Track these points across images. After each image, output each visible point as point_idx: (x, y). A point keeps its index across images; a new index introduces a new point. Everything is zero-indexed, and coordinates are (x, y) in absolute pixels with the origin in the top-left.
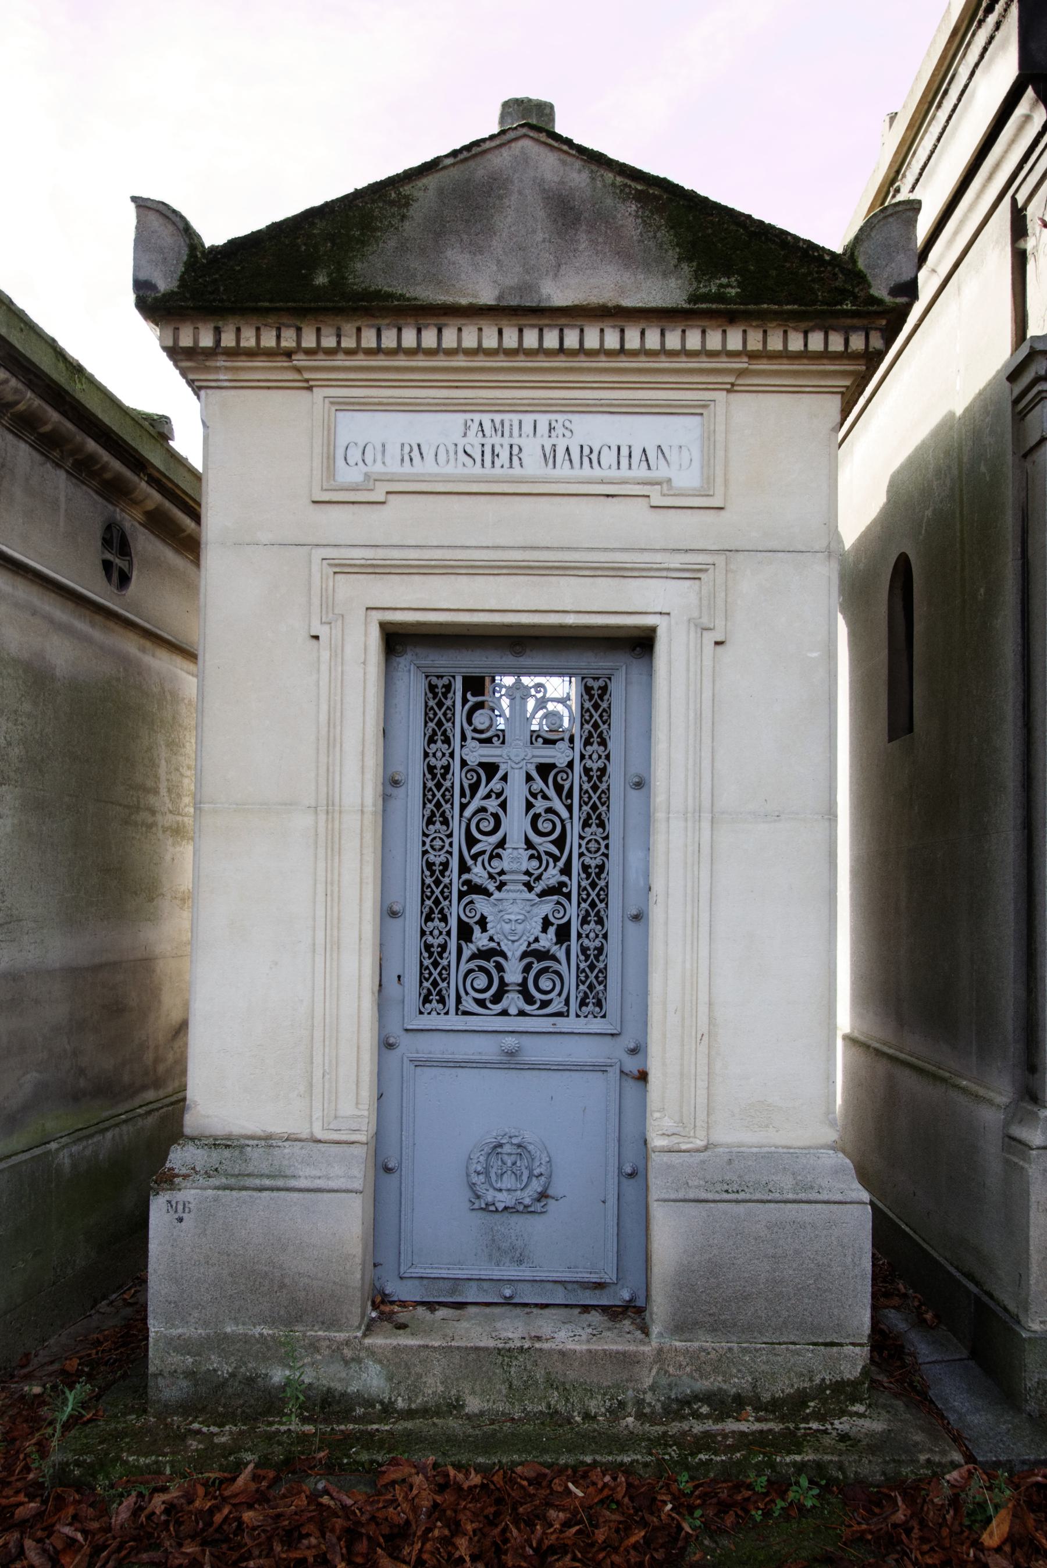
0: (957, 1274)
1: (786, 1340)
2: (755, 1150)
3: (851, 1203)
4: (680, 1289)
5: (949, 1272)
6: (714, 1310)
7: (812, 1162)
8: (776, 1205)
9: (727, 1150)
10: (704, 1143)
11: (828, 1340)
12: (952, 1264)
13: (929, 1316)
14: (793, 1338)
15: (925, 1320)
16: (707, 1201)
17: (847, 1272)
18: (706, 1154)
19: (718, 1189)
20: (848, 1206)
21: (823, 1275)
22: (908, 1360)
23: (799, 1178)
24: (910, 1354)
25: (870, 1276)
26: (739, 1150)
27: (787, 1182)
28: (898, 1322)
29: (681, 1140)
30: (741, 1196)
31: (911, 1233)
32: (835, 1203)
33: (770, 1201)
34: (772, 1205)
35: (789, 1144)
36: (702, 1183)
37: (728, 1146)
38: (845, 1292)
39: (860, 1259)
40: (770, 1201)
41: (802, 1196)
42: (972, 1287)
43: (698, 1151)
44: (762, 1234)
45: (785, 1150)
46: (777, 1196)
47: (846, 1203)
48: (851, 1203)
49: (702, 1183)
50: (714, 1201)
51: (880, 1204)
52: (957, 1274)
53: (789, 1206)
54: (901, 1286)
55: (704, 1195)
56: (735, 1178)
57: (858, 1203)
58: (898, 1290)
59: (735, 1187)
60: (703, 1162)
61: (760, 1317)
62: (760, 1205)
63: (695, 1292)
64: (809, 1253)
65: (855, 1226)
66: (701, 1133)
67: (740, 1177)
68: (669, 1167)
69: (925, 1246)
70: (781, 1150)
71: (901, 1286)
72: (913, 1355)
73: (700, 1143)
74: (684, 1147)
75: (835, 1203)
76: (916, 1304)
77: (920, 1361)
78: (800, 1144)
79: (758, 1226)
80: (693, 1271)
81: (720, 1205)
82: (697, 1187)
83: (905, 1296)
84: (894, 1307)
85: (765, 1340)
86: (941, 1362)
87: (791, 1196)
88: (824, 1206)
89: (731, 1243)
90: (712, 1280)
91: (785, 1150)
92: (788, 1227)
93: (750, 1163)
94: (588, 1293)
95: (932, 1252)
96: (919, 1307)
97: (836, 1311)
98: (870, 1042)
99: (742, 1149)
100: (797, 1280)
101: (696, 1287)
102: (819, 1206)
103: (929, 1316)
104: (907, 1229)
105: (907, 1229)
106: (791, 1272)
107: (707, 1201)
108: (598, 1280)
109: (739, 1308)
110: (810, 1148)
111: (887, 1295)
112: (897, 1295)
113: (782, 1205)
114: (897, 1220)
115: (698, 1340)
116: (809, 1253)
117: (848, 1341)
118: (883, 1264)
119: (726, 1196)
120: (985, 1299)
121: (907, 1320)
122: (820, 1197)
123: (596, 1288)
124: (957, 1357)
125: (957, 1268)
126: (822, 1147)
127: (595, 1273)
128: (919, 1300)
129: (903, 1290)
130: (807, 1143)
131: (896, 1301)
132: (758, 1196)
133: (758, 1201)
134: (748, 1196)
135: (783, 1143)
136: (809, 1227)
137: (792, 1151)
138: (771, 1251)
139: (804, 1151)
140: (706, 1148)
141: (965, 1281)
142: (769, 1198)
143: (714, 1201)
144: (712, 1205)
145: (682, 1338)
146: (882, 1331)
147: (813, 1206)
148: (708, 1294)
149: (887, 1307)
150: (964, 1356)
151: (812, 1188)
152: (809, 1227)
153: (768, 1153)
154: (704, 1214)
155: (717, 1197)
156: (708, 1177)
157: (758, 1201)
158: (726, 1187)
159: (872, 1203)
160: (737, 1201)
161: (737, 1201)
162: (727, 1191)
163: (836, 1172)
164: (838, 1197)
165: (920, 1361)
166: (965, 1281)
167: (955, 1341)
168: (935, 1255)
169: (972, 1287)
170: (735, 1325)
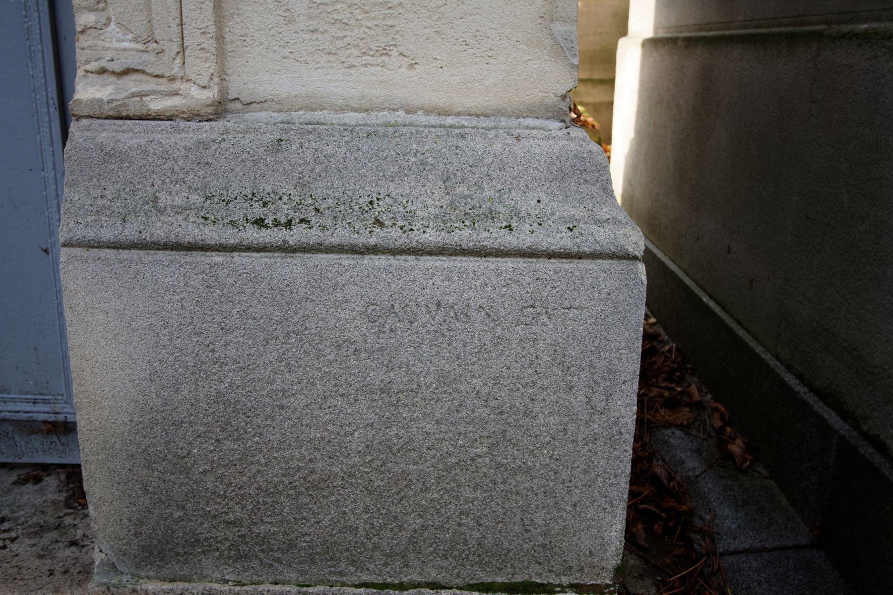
0: (802, 390)
1: (415, 577)
2: (351, 118)
3: (594, 256)
4: (149, 466)
5: (784, 383)
6: (236, 513)
7: (497, 147)
8: (395, 261)
9: (280, 117)
10: (211, 95)
11: (518, 579)
12: (789, 368)
13: (736, 448)
14: (433, 575)
15: (730, 456)
16: (204, 248)
17: (571, 427)
18: (219, 125)
19: (238, 216)
20: (585, 264)
21: (512, 432)
22: (699, 543)
23: (461, 189)
24: (704, 533)
25: (629, 438)
26: (309, 116)
27: (428, 199)
28: (682, 451)
29: (151, 85)
30: (297, 235)
31: (717, 309)
32: (551, 255)
33: (374, 250)
34: (381, 261)
35: (441, 100)
36: (196, 199)
37: (281, 105)
38: (564, 474)
39: (609, 396)
40: (374, 250)
41: (463, 236)
42: (833, 418)
43: (194, 116)
44: (354, 335)
45: (433, 119)
46: (393, 235)
47: (580, 256)
48: (594, 256)
49: (196, 199)
50: (221, 248)
51: (660, 255)
52: (802, 390)
53: (428, 262)
54: (694, 389)
55: (193, 232)
56: (288, 188)
57: (613, 256)
58: (690, 395)
59: (284, 211)
60: (205, 145)
61: (354, 530)
62: (347, 260)
63: (187, 472)
64: (476, 382)
65: (603, 325)
66: (201, 67)
67: (301, 185)
68: (110, 155)
69: (741, 332)
70: (421, 118)
71: (694, 389)
72: (708, 535)
73: (199, 96)
74: (156, 105)
75: (551, 255)
76: (718, 423)
77: (721, 547)
78: (473, 102)
79: (343, 314)
80: (178, 425)
81: (238, 258)
82: (180, 210)
83: (699, 406)
84: (681, 427)
85: (365, 578)
86: (760, 551)
87: (431, 237)
88: (521, 264)
89: (273, 356)
90: (229, 445)
91: (433, 119)
92: (423, 317)
93: (330, 150)
94: (37, 441)
95: (753, 343)
96: (722, 429)
97: (539, 518)
98: (675, 35)
99: (318, 115)
100: (445, 446)
101: (189, 462)
102: (507, 264)
103: (736, 448)
104: (712, 304)
105: (712, 304)
106: (429, 427)
107: (204, 248)
108: (51, 418)
109: (299, 508)
110: (498, 113)
111: (672, 404)
112: (687, 405)
113: (411, 260)
114: (696, 290)
115: (202, 578)
116: (476, 382)
117: (565, 580)
118: (670, 351)
119: (253, 235)
120: (866, 450)
121: (699, 452)
122: (511, 241)
123: (49, 432)
124: (789, 542)
125: (800, 377)
126: (533, 111)
127: (45, 402)
128: (722, 418)
129: (697, 396)
130: (493, 101)
131: (685, 415)
132: (342, 235)
133: (341, 249)
134: (313, 236)
135: (428, 98)
136: (478, 317)
137: (450, 121)
138: (377, 377)
139: (484, 123)
140: (219, 110)
141: (820, 407)
142: (373, 241)
143: (221, 248)
144: (217, 258)
145: (165, 572)
146: (655, 480)
147: (492, 263)
148: (221, 478)
149: (669, 425)
150: (804, 541)
151: (491, 215)
152: (478, 317)
153: (387, 125)
154: (196, 281)
155: (230, 236)
156: (215, 186)
157: (341, 249)
158: (258, 211)
159: (649, 258)
160: (285, 249)
161: (285, 249)
162: (260, 223)
163: (562, 175)
164: (562, 240)
165: (721, 547)
166: (820, 407)
167: (784, 502)
168: (758, 349)
169: (833, 418)
170: (292, 545)
